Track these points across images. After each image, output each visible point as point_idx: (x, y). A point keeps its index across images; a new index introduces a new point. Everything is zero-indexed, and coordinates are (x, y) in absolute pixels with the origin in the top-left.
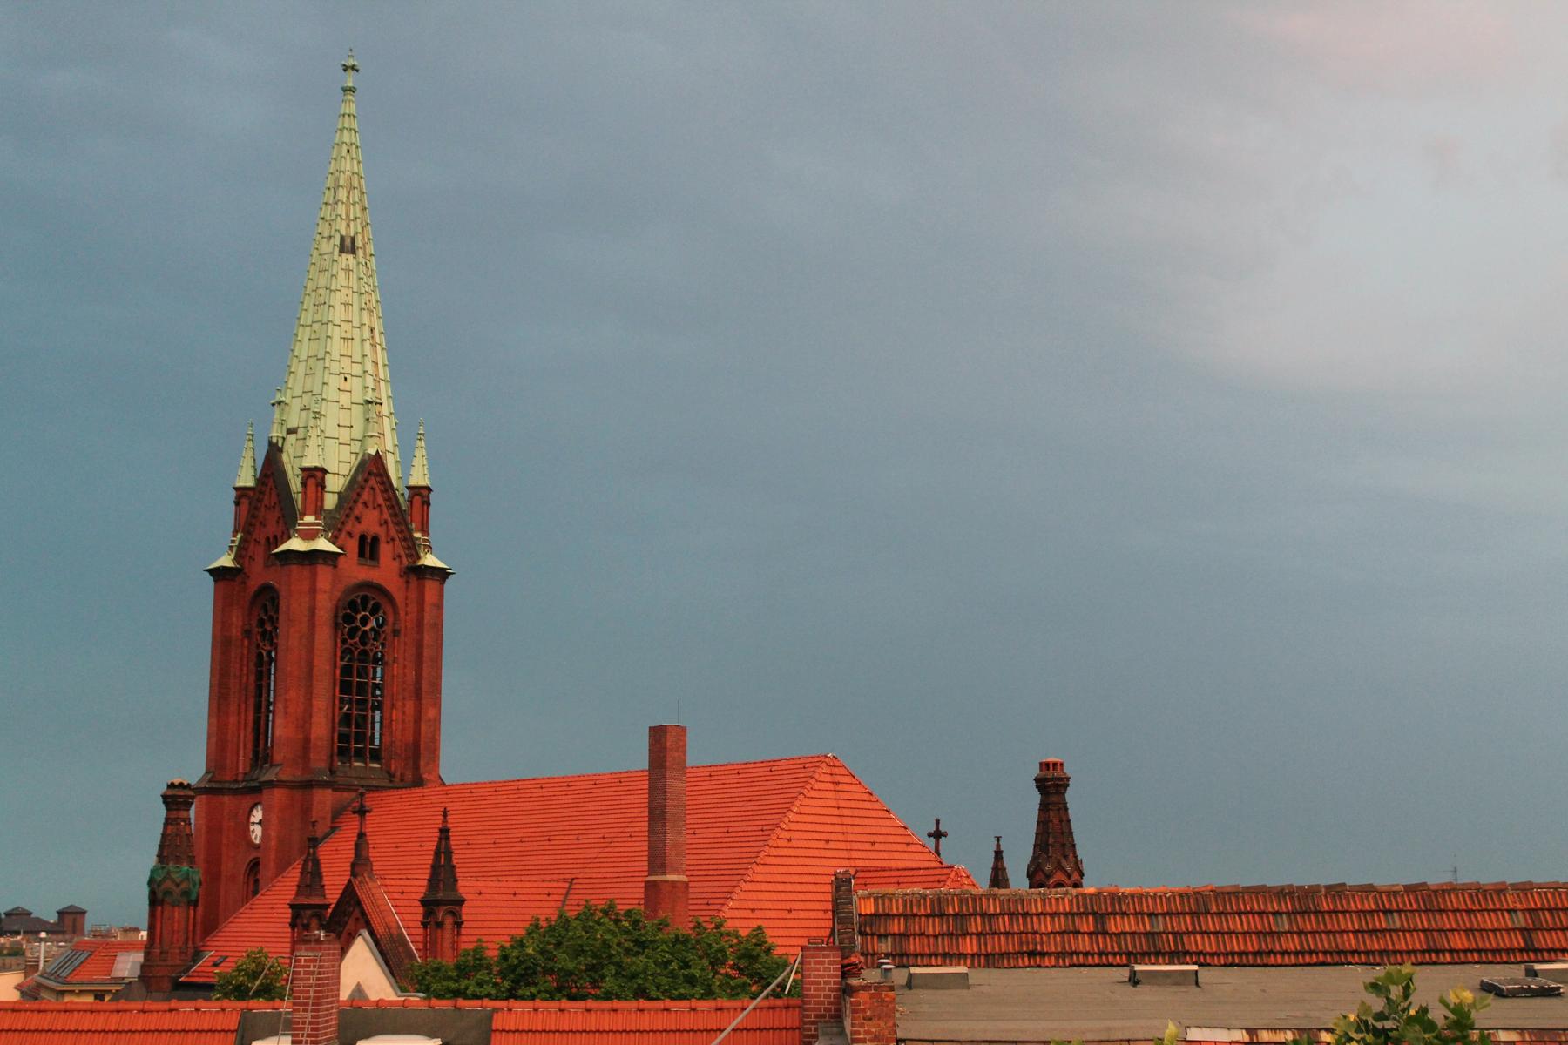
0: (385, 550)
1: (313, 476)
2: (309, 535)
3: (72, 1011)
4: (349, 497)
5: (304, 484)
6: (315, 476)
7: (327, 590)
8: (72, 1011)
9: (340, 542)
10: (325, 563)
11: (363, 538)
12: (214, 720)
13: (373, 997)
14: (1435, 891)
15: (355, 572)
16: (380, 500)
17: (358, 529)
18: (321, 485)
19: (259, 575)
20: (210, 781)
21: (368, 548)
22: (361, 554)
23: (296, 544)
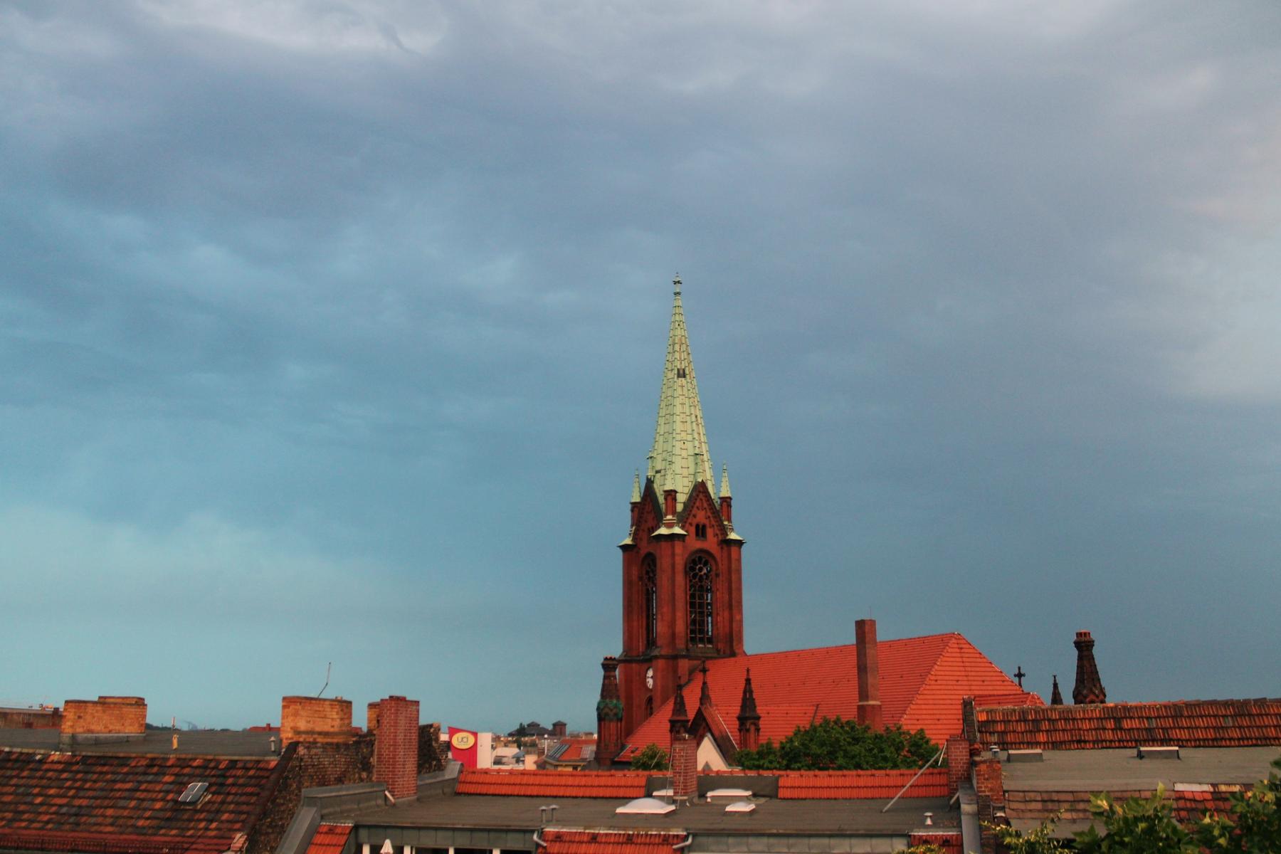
0: (709, 532)
2: (670, 526)
7: (681, 555)
11: (697, 526)
15: (697, 544)
16: (705, 505)
17: (695, 521)
18: (675, 499)
19: (645, 548)
21: (701, 531)
22: (697, 534)
23: (663, 531)
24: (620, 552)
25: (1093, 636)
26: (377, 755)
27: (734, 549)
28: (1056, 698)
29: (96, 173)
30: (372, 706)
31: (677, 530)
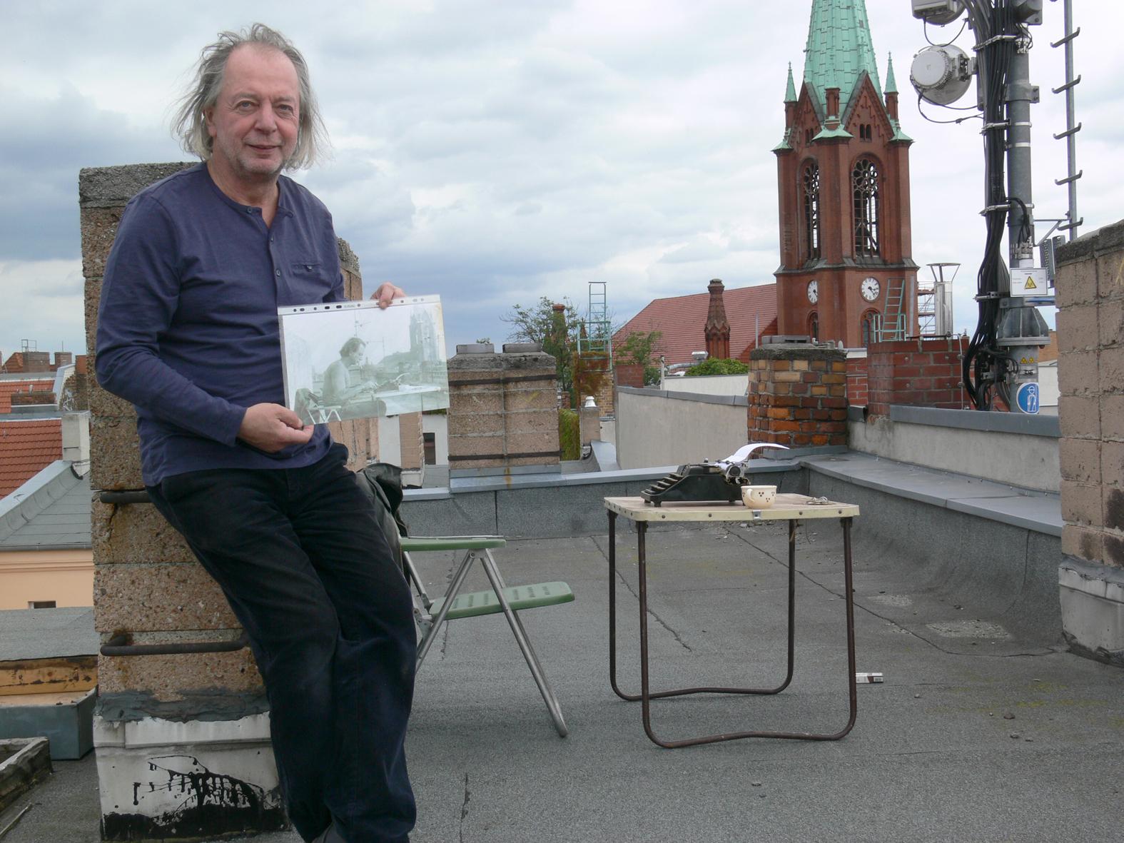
0: (874, 133)
1: (833, 93)
2: (833, 127)
3: (990, 431)
4: (855, 99)
5: (828, 98)
6: (833, 94)
7: (846, 156)
8: (990, 431)
9: (850, 130)
10: (843, 143)
11: (862, 126)
12: (784, 213)
13: (73, 373)
14: (1064, 634)
15: (862, 147)
16: (869, 103)
17: (858, 122)
18: (837, 98)
19: (805, 153)
20: (784, 270)
21: (865, 132)
22: (862, 136)
23: (825, 133)
24: (775, 157)
25: (723, 283)
26: (1058, 373)
27: (901, 150)
28: (1120, 299)
29: (157, 352)
30: (76, 356)
31: (841, 132)
